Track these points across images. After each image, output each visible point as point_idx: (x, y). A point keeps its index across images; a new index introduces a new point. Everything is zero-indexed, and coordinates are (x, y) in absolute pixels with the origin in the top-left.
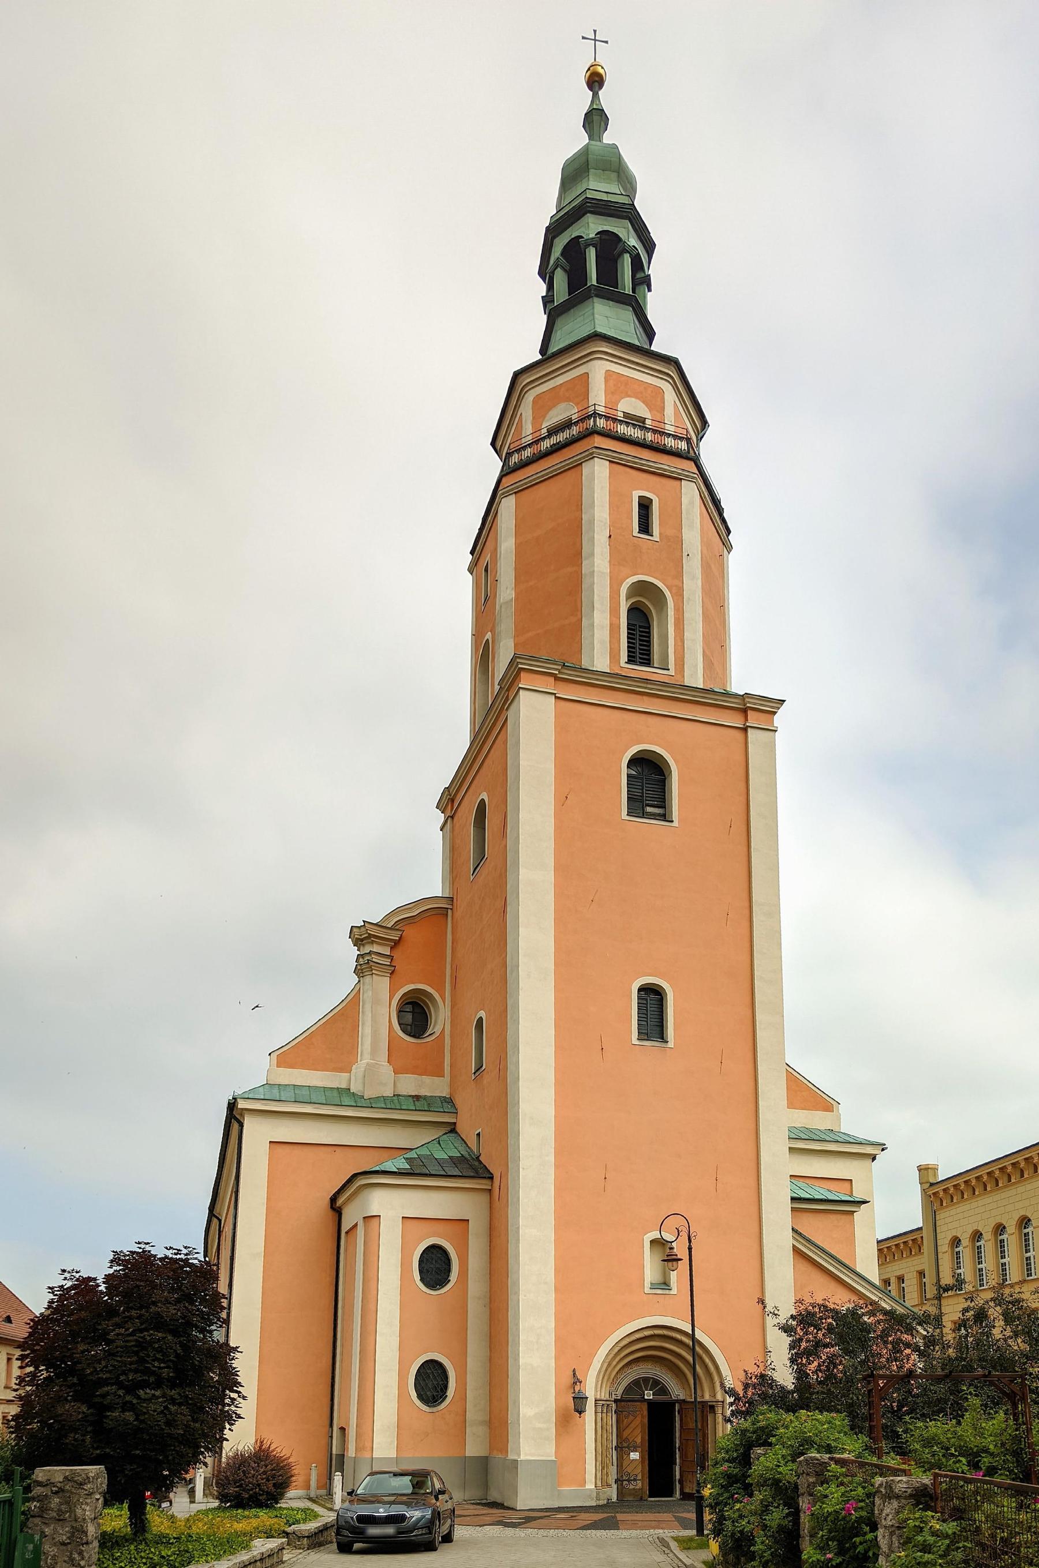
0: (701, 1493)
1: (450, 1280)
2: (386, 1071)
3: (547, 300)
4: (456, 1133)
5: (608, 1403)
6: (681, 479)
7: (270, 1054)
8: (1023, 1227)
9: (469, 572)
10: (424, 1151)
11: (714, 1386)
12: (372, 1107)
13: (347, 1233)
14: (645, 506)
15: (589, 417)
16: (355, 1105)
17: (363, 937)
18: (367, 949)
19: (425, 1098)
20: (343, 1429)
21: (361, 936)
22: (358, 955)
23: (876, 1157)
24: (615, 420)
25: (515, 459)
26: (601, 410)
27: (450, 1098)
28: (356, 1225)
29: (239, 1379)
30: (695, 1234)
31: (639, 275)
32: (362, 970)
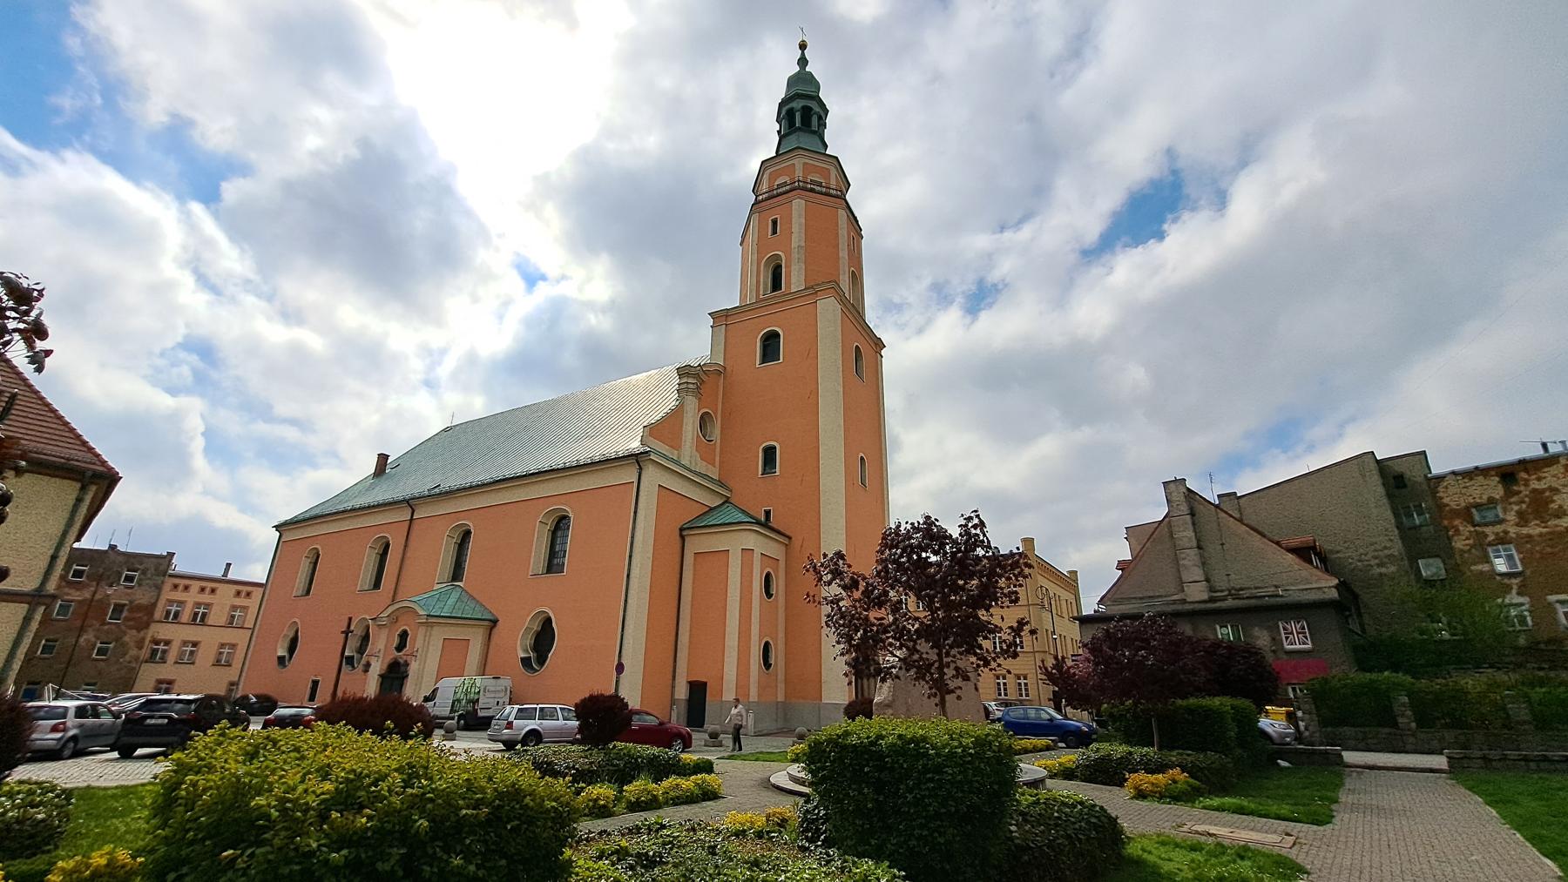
0: (92, 864)
3: (779, 132)
11: (786, 602)
18: (685, 380)
21: (684, 372)
25: (760, 198)
29: (120, 475)
31: (821, 122)
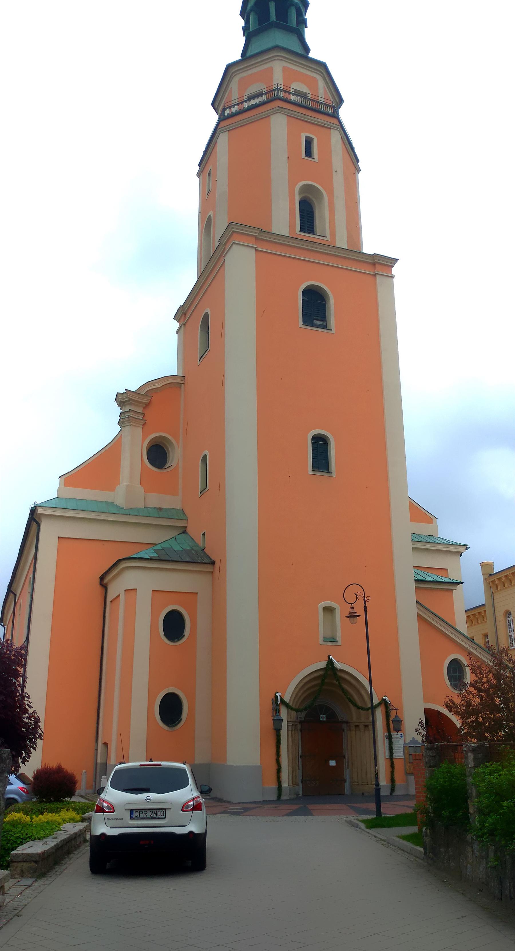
1: (184, 635)
2: (140, 490)
4: (187, 533)
5: (296, 723)
6: (330, 128)
7: (60, 477)
8: (507, 617)
9: (198, 176)
10: (166, 545)
12: (130, 515)
13: (111, 602)
14: (309, 143)
15: (274, 90)
16: (118, 513)
17: (125, 400)
19: (166, 510)
20: (106, 744)
22: (121, 412)
23: (462, 554)
24: (289, 93)
25: (227, 112)
26: (281, 87)
27: (182, 510)
28: (119, 595)
30: (369, 598)
32: (124, 422)
